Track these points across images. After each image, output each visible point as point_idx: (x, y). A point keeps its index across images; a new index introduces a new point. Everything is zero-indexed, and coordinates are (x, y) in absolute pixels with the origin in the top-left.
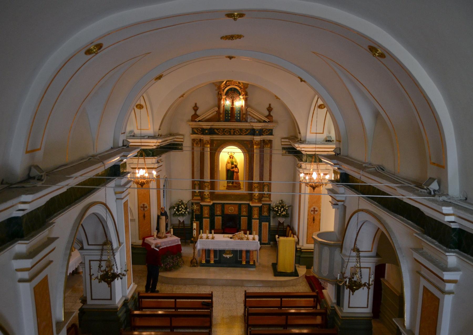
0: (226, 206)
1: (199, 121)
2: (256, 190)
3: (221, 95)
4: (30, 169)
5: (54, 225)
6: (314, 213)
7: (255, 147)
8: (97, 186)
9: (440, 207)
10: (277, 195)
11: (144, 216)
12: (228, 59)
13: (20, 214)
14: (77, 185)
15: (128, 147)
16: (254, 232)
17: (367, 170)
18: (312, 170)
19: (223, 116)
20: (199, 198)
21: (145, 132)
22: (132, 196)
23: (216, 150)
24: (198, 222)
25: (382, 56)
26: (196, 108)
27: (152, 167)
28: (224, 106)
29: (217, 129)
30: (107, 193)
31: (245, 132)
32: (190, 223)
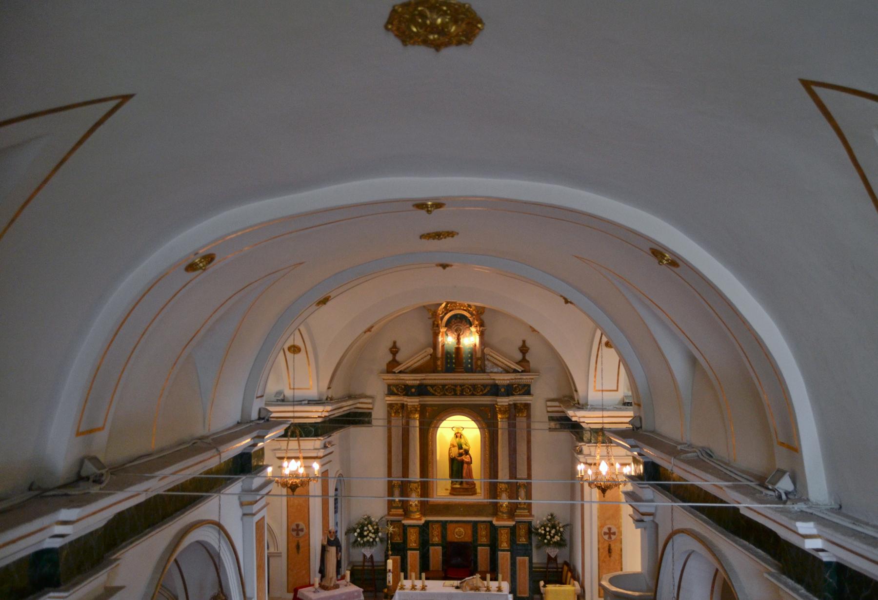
0: (450, 527)
1: (400, 372)
2: (504, 495)
3: (438, 326)
4: (81, 462)
5: (118, 562)
6: (610, 538)
7: (499, 416)
8: (207, 491)
9: (793, 522)
10: (543, 505)
11: (298, 547)
12: (441, 268)
13: (57, 543)
14: (169, 490)
15: (268, 420)
16: (500, 576)
17: (683, 456)
18: (598, 457)
19: (442, 362)
20: (401, 511)
21: (300, 394)
22: (275, 512)
23: (430, 424)
24: (399, 557)
25: (673, 264)
26: (394, 350)
27: (314, 455)
28: (443, 346)
29: (432, 386)
30: (225, 505)
31: (482, 391)
32: (383, 559)
